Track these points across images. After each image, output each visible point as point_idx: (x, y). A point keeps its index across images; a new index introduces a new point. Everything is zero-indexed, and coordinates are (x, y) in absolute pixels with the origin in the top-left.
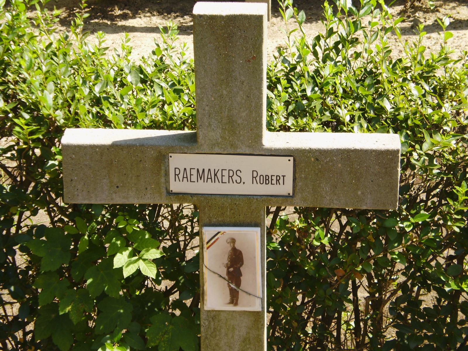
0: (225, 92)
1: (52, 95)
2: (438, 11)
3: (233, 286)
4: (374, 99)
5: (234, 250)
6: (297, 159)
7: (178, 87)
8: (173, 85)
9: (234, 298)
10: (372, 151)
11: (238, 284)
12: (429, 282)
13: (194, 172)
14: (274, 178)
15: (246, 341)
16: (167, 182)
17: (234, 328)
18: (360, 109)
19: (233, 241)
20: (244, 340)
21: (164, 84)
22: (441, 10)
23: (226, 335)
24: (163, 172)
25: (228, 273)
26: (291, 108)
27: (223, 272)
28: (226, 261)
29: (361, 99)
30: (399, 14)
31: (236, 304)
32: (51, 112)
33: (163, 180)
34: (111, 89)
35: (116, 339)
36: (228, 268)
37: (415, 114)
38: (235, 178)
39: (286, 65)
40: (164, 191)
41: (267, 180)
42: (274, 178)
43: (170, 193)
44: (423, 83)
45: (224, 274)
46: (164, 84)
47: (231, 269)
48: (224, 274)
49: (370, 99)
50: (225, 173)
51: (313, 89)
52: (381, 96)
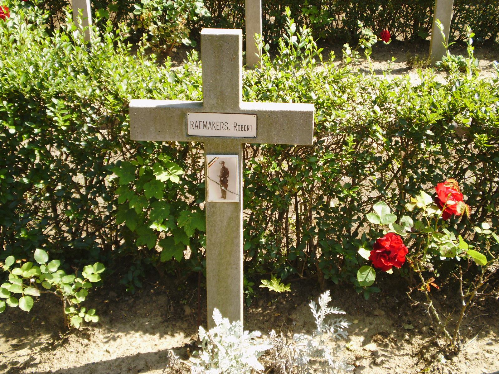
0: (218, 77)
1: (126, 87)
2: (361, 64)
3: (223, 188)
4: (306, 92)
5: (224, 167)
6: (259, 116)
7: (196, 84)
8: (194, 83)
9: (224, 194)
10: (299, 112)
11: (226, 187)
12: (334, 193)
13: (201, 123)
14: (246, 127)
15: (230, 218)
16: (187, 129)
17: (224, 212)
18: (298, 97)
19: (223, 163)
20: (230, 218)
21: (188, 83)
22: (362, 63)
23: (220, 215)
24: (184, 123)
25: (221, 181)
26: (260, 96)
27: (218, 180)
28: (219, 174)
29: (299, 92)
30: (338, 66)
31: (225, 198)
32: (125, 95)
33: (184, 128)
34: (159, 85)
35: (160, 222)
36: (221, 178)
37: (328, 100)
38: (224, 127)
39: (259, 73)
40: (184, 134)
41: (242, 128)
42: (246, 127)
43: (188, 136)
44: (334, 85)
45: (218, 182)
46: (188, 83)
47: (222, 179)
48: (218, 181)
49: (304, 92)
50: (219, 124)
51: (272, 86)
52: (310, 91)
